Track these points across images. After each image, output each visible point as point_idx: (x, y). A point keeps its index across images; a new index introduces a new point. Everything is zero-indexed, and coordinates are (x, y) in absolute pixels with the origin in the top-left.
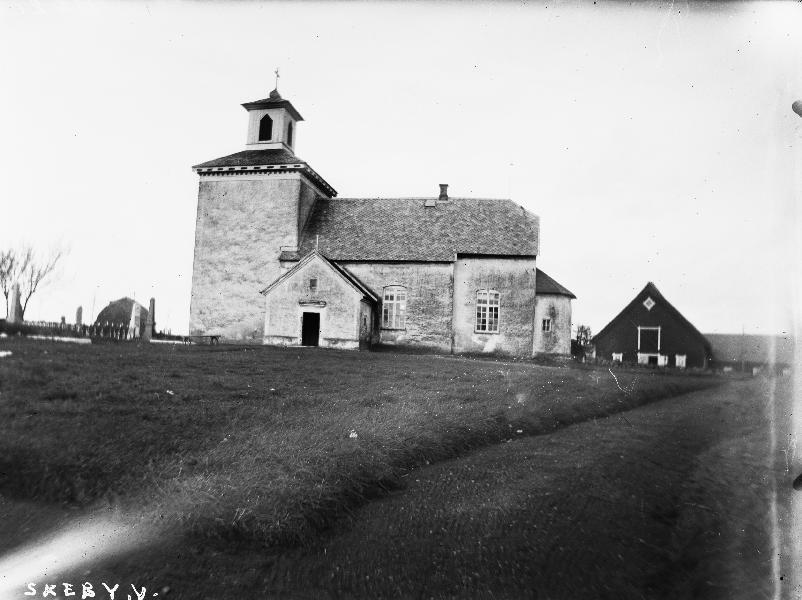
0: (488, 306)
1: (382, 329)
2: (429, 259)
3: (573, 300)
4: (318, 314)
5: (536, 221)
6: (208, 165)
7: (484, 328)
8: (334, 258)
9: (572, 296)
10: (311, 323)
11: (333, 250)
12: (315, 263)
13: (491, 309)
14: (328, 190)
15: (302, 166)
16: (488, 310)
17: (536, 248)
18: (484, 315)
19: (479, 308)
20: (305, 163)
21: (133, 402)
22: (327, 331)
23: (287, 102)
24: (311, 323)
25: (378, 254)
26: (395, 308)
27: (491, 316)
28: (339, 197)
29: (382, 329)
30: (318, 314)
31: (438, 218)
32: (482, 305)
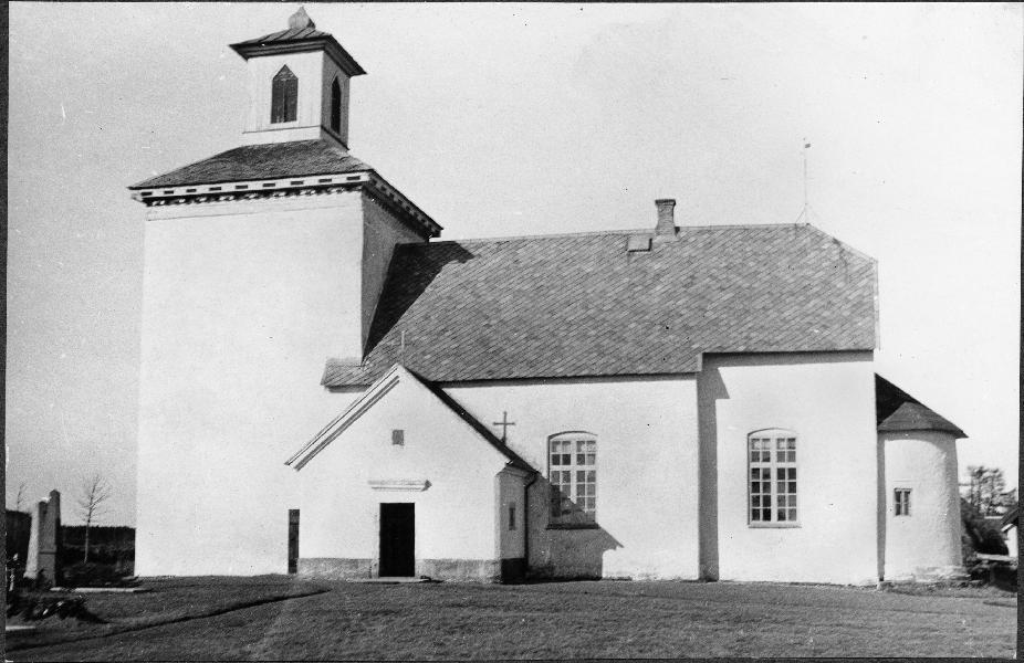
0: (774, 465)
1: (708, 575)
2: (641, 368)
3: (959, 442)
4: (412, 506)
5: (868, 269)
6: (167, 182)
7: (767, 516)
8: (440, 377)
9: (959, 434)
10: (397, 523)
11: (438, 357)
12: (406, 396)
13: (781, 473)
14: (413, 218)
15: (365, 177)
16: (774, 475)
17: (872, 332)
18: (767, 487)
19: (756, 471)
20: (372, 171)
21: (912, 622)
22: (429, 546)
23: (330, 38)
24: (397, 523)
25: (531, 364)
26: (574, 478)
27: (781, 488)
28: (445, 237)
29: (708, 575)
30: (412, 506)
31: (658, 276)
32: (761, 465)
